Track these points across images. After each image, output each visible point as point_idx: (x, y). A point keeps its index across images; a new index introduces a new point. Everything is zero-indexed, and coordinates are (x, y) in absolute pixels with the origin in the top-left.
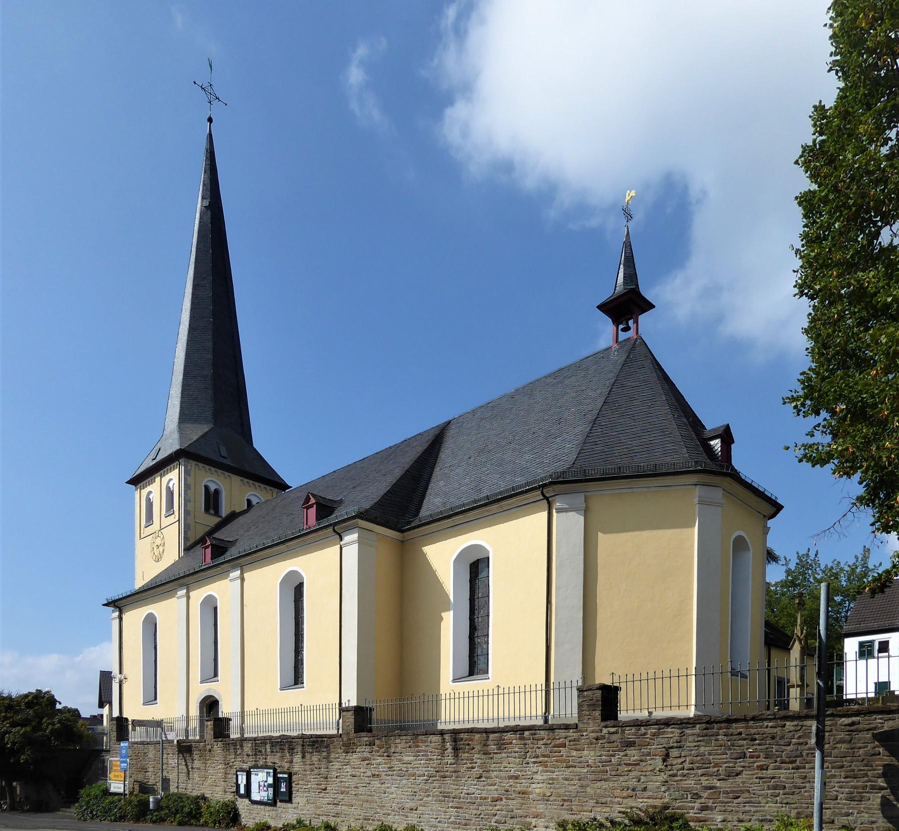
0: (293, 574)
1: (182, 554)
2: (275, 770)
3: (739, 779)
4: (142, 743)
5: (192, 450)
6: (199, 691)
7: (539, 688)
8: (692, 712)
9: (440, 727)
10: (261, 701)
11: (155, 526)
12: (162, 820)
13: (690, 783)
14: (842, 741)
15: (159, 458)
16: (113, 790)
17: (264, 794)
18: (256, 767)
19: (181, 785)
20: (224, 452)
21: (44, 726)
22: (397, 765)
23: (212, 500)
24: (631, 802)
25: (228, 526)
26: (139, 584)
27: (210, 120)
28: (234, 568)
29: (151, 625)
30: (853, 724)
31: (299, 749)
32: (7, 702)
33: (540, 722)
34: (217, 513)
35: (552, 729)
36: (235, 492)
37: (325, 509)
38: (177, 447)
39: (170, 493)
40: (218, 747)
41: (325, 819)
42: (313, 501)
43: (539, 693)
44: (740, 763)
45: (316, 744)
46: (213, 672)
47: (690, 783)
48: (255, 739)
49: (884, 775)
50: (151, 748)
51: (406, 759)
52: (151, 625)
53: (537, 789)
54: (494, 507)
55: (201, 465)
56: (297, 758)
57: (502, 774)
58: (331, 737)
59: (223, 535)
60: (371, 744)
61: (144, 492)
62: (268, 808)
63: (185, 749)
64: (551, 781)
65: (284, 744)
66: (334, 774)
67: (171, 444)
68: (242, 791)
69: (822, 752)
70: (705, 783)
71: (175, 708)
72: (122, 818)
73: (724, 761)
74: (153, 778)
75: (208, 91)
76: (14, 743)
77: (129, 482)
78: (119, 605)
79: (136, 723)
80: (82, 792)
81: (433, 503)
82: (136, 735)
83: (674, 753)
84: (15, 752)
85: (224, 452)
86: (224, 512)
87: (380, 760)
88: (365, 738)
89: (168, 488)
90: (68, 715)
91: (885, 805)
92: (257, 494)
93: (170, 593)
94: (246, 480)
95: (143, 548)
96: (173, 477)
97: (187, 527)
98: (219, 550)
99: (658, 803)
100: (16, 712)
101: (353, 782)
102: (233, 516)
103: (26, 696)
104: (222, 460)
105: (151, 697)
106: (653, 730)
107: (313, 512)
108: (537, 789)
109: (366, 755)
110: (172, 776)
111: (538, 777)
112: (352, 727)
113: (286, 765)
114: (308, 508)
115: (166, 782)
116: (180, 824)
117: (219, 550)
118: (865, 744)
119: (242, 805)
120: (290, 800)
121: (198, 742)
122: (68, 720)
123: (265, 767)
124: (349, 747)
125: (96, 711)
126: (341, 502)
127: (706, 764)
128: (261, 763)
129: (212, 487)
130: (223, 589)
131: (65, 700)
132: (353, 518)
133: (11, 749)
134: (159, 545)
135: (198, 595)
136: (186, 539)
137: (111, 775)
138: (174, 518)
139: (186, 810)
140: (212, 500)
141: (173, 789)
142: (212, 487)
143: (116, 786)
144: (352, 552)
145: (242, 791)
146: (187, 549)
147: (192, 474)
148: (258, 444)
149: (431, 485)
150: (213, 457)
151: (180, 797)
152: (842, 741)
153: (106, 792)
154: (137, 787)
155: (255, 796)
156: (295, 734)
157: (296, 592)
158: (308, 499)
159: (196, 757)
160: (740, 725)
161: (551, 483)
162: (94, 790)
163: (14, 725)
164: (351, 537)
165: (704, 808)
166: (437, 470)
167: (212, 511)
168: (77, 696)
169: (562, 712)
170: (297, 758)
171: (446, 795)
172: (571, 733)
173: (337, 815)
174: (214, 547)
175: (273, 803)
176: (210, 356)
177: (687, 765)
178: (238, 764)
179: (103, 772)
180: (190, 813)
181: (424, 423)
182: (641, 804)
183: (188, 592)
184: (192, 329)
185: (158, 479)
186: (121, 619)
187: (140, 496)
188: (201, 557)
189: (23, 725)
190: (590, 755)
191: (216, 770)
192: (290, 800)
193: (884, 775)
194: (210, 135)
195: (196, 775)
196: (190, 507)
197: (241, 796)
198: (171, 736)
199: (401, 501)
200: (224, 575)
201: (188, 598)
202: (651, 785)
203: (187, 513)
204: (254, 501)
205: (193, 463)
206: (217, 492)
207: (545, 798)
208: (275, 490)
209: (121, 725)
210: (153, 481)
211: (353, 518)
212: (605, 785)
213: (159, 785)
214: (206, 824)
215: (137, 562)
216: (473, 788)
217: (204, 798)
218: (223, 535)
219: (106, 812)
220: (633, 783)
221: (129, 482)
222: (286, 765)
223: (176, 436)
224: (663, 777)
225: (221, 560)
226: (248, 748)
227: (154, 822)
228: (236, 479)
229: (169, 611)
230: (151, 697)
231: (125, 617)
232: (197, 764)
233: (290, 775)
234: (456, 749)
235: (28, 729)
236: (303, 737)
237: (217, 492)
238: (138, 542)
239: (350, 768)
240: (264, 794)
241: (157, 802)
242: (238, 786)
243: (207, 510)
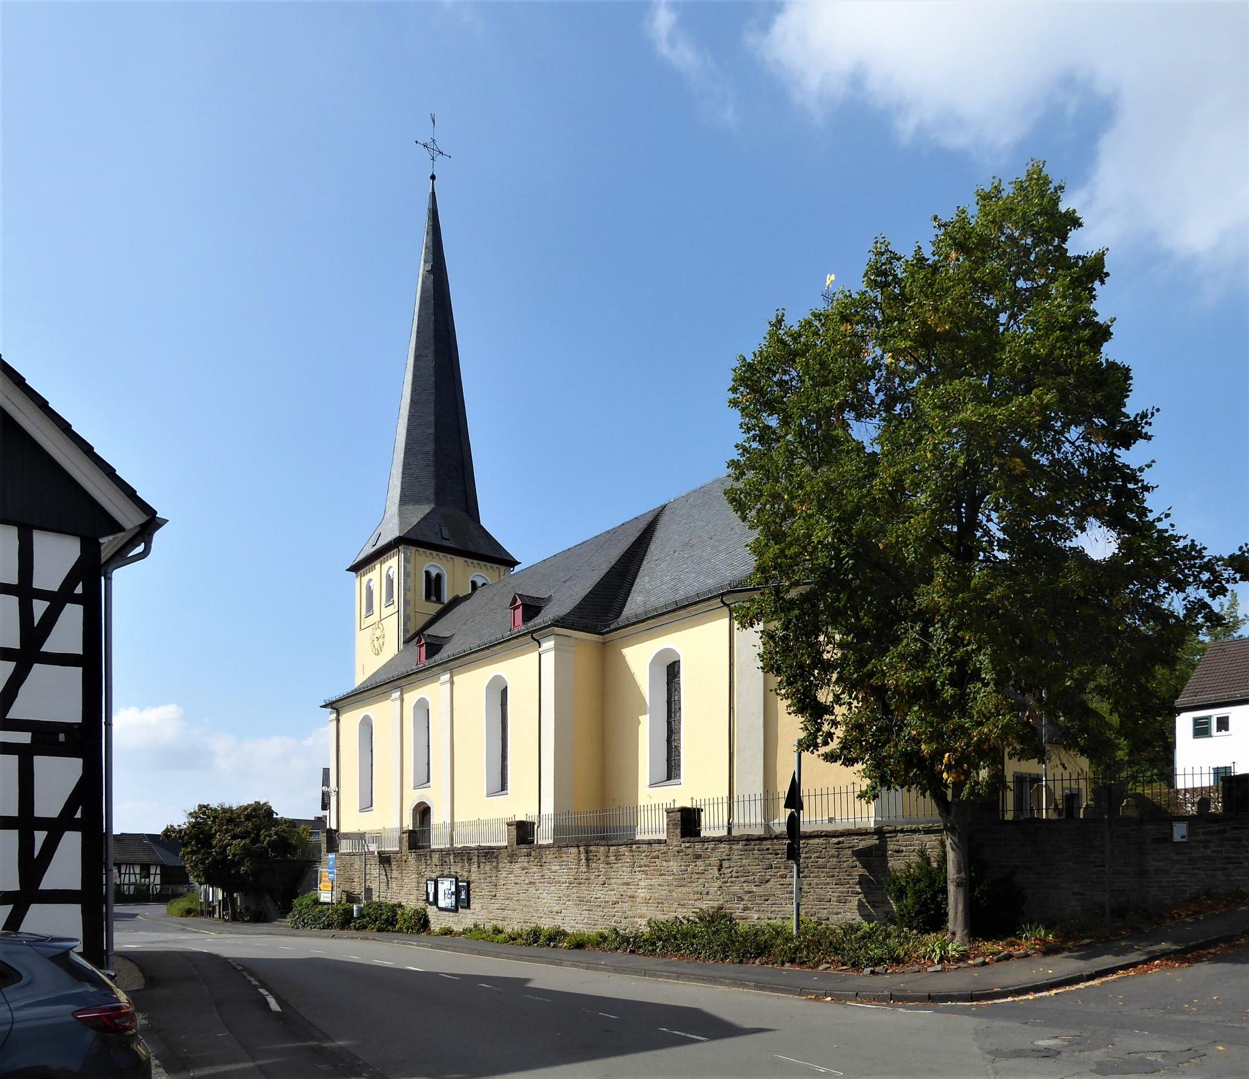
0: (497, 679)
1: (401, 647)
2: (457, 879)
3: (768, 885)
4: (349, 854)
5: (412, 536)
6: (413, 797)
7: (758, 797)
8: (551, 841)
9: (638, 837)
10: (472, 812)
11: (375, 618)
12: (365, 927)
13: (736, 888)
14: (833, 856)
15: (379, 545)
16: (322, 899)
17: (448, 901)
18: (442, 876)
19: (382, 894)
20: (446, 534)
21: (262, 838)
22: (547, 874)
23: (433, 586)
24: (699, 904)
25: (449, 615)
26: (359, 679)
27: (433, 177)
28: (444, 671)
29: (367, 724)
30: (839, 843)
31: (475, 859)
32: (228, 814)
33: (724, 833)
34: (439, 600)
35: (737, 840)
36: (457, 575)
37: (531, 608)
38: (396, 534)
39: (390, 582)
40: (412, 858)
41: (494, 922)
42: (519, 602)
43: (758, 803)
44: (770, 872)
45: (488, 854)
46: (425, 780)
47: (736, 888)
48: (441, 850)
49: (860, 883)
50: (357, 858)
51: (554, 868)
52: (367, 724)
53: (642, 893)
54: (683, 612)
55: (421, 550)
56: (474, 868)
57: (619, 881)
58: (499, 848)
59: (437, 630)
60: (529, 855)
61: (365, 579)
62: (452, 914)
63: (385, 859)
64: (650, 887)
65: (464, 855)
66: (502, 882)
67: (391, 531)
68: (431, 899)
69: (798, 865)
70: (746, 889)
71: (386, 820)
72: (329, 926)
73: (757, 870)
74: (358, 889)
75: (433, 150)
76: (234, 855)
77: (350, 570)
78: (336, 706)
79: (347, 836)
80: (295, 901)
81: (636, 602)
82: (345, 846)
83: (726, 864)
84: (236, 864)
85: (446, 534)
86: (446, 598)
87: (535, 869)
88: (524, 849)
89: (388, 576)
90: (284, 827)
91: (861, 906)
92: (481, 573)
93: (385, 696)
94: (470, 561)
95: (363, 640)
96: (393, 564)
97: (407, 618)
98: (434, 647)
99: (716, 904)
100: (237, 825)
101: (515, 889)
102: (456, 601)
103: (246, 808)
104: (446, 543)
105: (367, 805)
106: (711, 845)
107: (519, 612)
108: (642, 893)
109: (526, 864)
110: (374, 886)
111: (642, 883)
112: (515, 840)
113: (466, 874)
114: (515, 609)
115: (369, 891)
116: (379, 930)
117: (434, 647)
118: (849, 860)
119: (431, 911)
120: (468, 907)
121: (396, 853)
122: (284, 831)
123: (449, 876)
124: (512, 858)
125: (321, 813)
126: (549, 599)
127: (747, 873)
128: (446, 872)
129: (434, 573)
130: (434, 692)
131: (284, 810)
132: (548, 626)
133: (232, 860)
134: (378, 641)
135: (412, 697)
136: (406, 631)
137: (321, 886)
138: (393, 609)
139: (384, 917)
140: (433, 586)
141: (375, 898)
142: (434, 573)
143: (325, 897)
144: (549, 659)
145: (431, 899)
146: (407, 642)
147: (412, 561)
148: (485, 522)
149: (638, 580)
150: (435, 541)
151: (380, 905)
152: (833, 856)
153: (317, 902)
154: (344, 897)
155: (442, 904)
156: (473, 845)
157: (501, 695)
158: (514, 601)
159: (394, 867)
160: (769, 842)
161: (729, 592)
162: (306, 900)
163: (234, 837)
164: (548, 644)
165: (746, 909)
166: (645, 562)
167: (434, 598)
168: (293, 804)
169: (819, 818)
170: (474, 868)
171: (581, 899)
172: (662, 847)
173: (504, 919)
174: (430, 646)
175: (455, 910)
176: (432, 431)
177: (734, 874)
178: (428, 874)
179: (314, 884)
180: (387, 920)
181: (642, 507)
182: (707, 905)
183: (402, 694)
184: (414, 403)
185: (378, 567)
186: (338, 721)
187: (359, 583)
188: (416, 658)
189: (243, 838)
190: (674, 865)
191: (410, 879)
192: (468, 907)
193: (860, 883)
194: (433, 193)
195: (394, 885)
196: (410, 596)
197: (431, 904)
198: (373, 848)
199: (603, 606)
200: (435, 677)
201: (402, 700)
202: (712, 890)
203: (406, 602)
204: (480, 582)
205: (413, 549)
206: (439, 577)
207: (646, 902)
208: (503, 568)
209: (333, 838)
210: (373, 568)
211: (548, 626)
212: (684, 890)
213: (362, 896)
214: (400, 931)
215: (357, 656)
216: (599, 893)
217: (400, 906)
218: (437, 630)
219: (316, 920)
220: (700, 888)
221: (350, 570)
222: (466, 874)
223: (396, 520)
224: (718, 884)
225: (437, 658)
226: (436, 857)
227: (358, 929)
228: (459, 561)
229: (383, 712)
230: (367, 805)
231: (343, 718)
232: (395, 874)
233: (468, 883)
234: (587, 860)
235: (248, 841)
236: (479, 848)
237: (439, 577)
238: (358, 633)
239: (514, 875)
240: (448, 901)
241: (360, 910)
242: (428, 894)
243: (428, 597)
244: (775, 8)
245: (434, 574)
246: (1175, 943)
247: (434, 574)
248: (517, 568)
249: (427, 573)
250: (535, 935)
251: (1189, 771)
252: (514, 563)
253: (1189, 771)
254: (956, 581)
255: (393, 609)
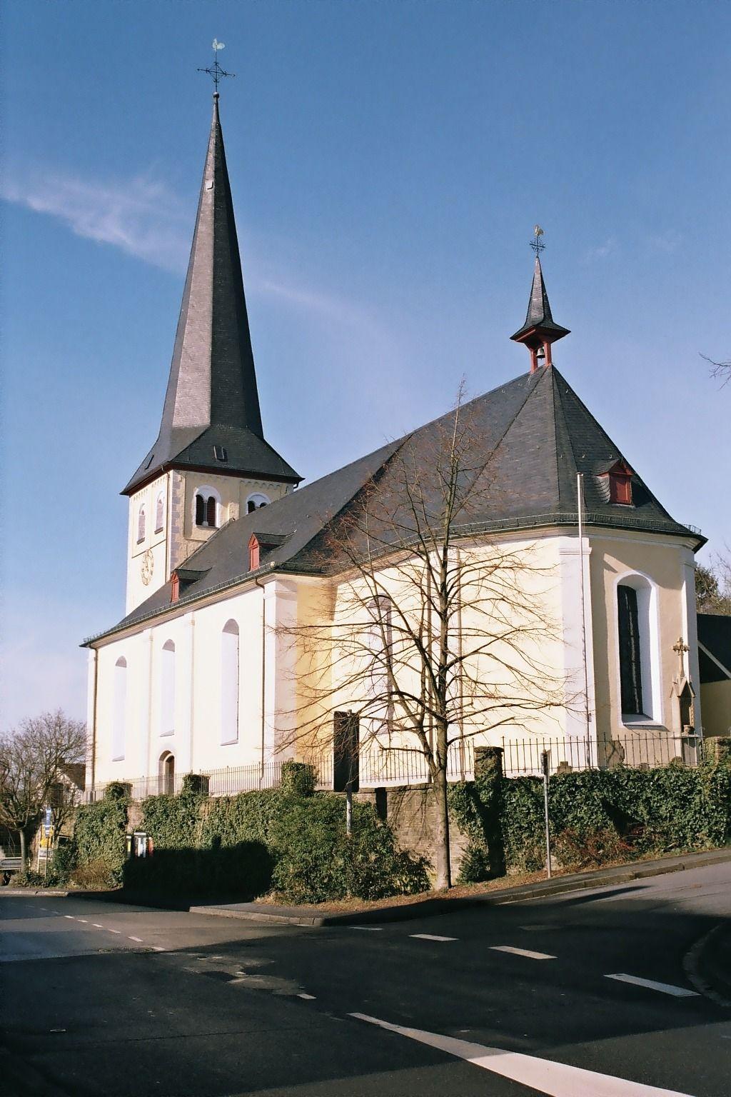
5: (187, 460)
26: (130, 608)
77: (512, 338)
95: (134, 567)
96: (160, 489)
164: (271, 587)
167: (205, 523)
221: (512, 338)
244: (728, 369)
245: (206, 498)
246: (521, 929)
247: (206, 498)
248: (302, 485)
249: (199, 498)
250: (251, 946)
251: (514, 742)
252: (298, 480)
253: (514, 742)
254: (273, 880)
255: (162, 536)
